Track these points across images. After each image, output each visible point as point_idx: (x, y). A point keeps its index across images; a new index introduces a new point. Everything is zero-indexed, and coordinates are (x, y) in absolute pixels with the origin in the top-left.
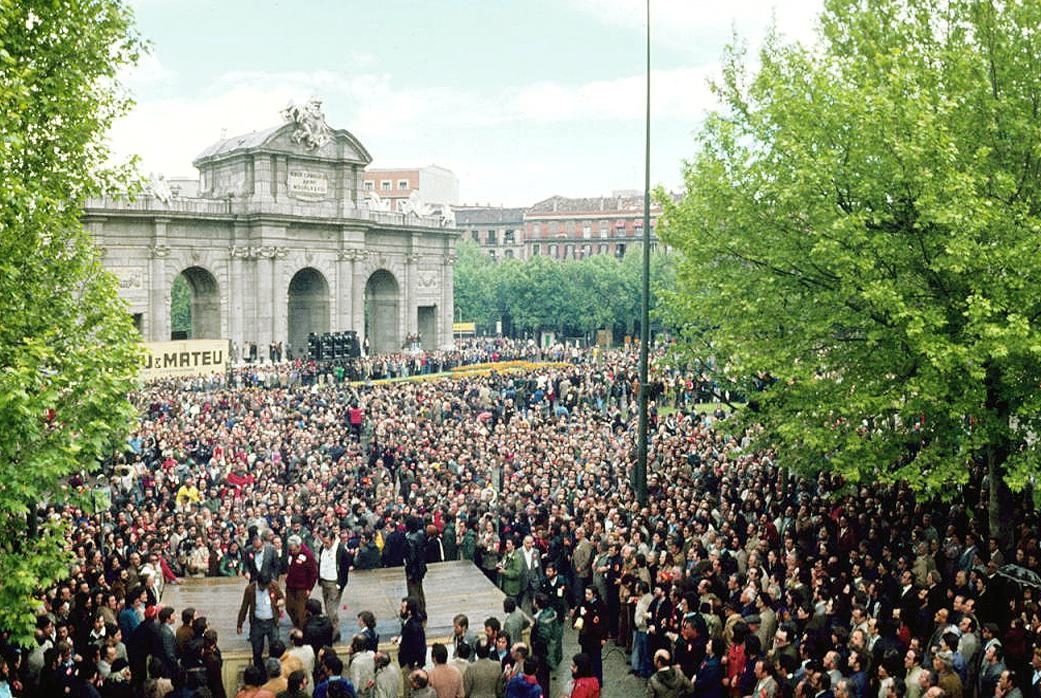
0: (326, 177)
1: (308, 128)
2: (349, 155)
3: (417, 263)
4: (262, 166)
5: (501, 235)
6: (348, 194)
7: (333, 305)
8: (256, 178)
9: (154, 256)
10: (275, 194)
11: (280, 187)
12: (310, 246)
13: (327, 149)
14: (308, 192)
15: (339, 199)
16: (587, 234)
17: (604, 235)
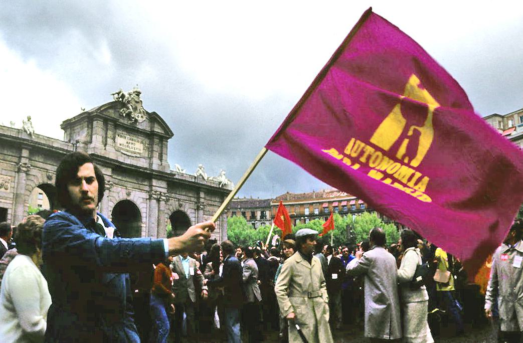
0: (142, 143)
1: (130, 107)
2: (158, 129)
3: (202, 209)
4: (98, 125)
5: (258, 214)
6: (156, 155)
7: (143, 229)
8: (94, 133)
9: (19, 171)
10: (105, 145)
11: (110, 141)
12: (129, 185)
13: (143, 124)
14: (129, 149)
15: (150, 158)
16: (307, 212)
17: (317, 212)
